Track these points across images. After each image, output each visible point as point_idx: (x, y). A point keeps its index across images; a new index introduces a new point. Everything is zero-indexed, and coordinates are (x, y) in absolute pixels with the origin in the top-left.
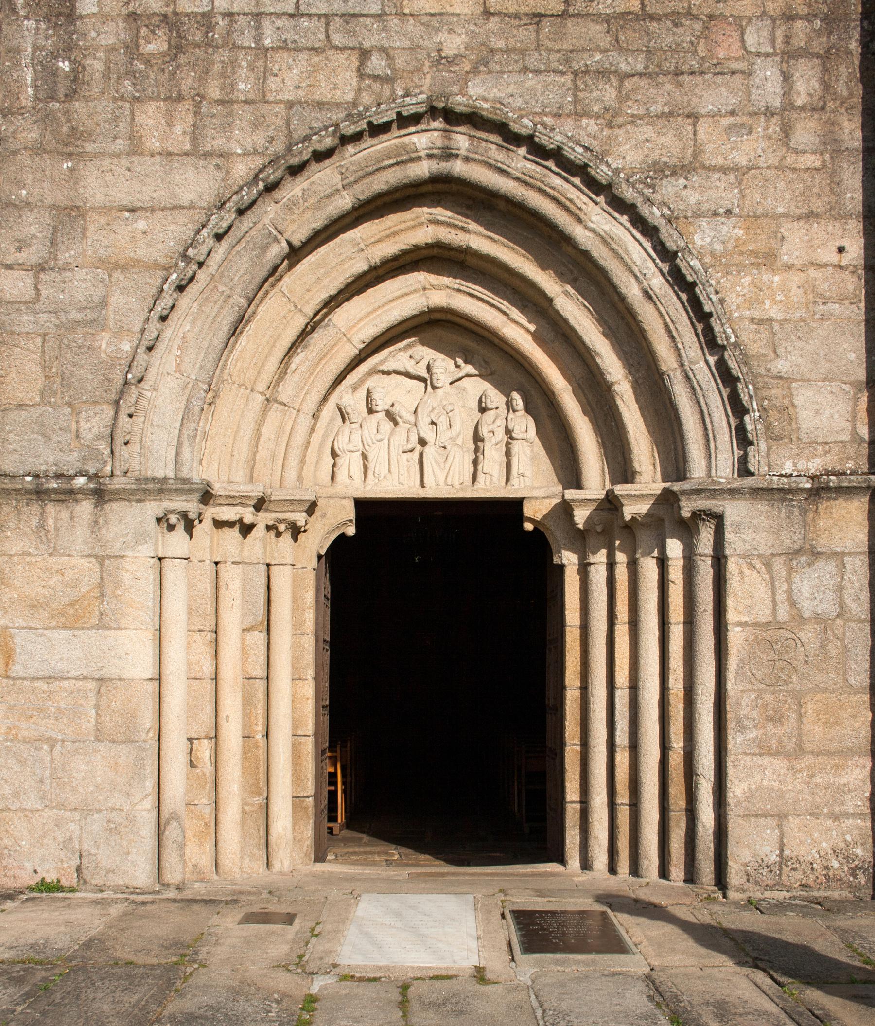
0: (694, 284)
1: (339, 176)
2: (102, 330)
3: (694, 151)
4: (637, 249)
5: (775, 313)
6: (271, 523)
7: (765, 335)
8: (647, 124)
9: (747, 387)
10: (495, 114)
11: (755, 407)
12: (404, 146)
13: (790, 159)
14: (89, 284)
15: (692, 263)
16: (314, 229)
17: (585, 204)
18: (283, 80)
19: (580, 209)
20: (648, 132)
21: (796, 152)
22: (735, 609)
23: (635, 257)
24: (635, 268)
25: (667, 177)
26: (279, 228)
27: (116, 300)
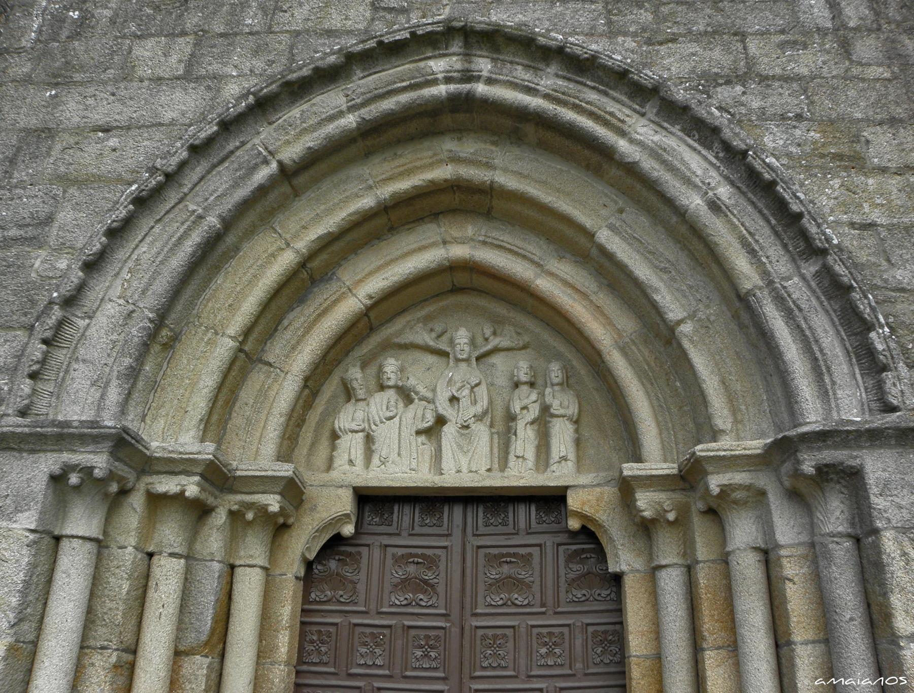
0: (773, 184)
1: (345, 99)
2: (40, 248)
3: (747, 63)
4: (695, 161)
5: (876, 216)
6: (235, 508)
7: (871, 241)
8: (690, 41)
9: (866, 297)
10: (521, 30)
11: (882, 320)
12: (418, 70)
13: (856, 71)
14: (39, 201)
15: (767, 160)
16: (309, 148)
17: (628, 116)
18: (293, 14)
19: (623, 122)
20: (694, 48)
21: (860, 64)
22: (906, 612)
23: (694, 166)
24: (696, 178)
25: (721, 85)
26: (271, 148)
27: (65, 216)
